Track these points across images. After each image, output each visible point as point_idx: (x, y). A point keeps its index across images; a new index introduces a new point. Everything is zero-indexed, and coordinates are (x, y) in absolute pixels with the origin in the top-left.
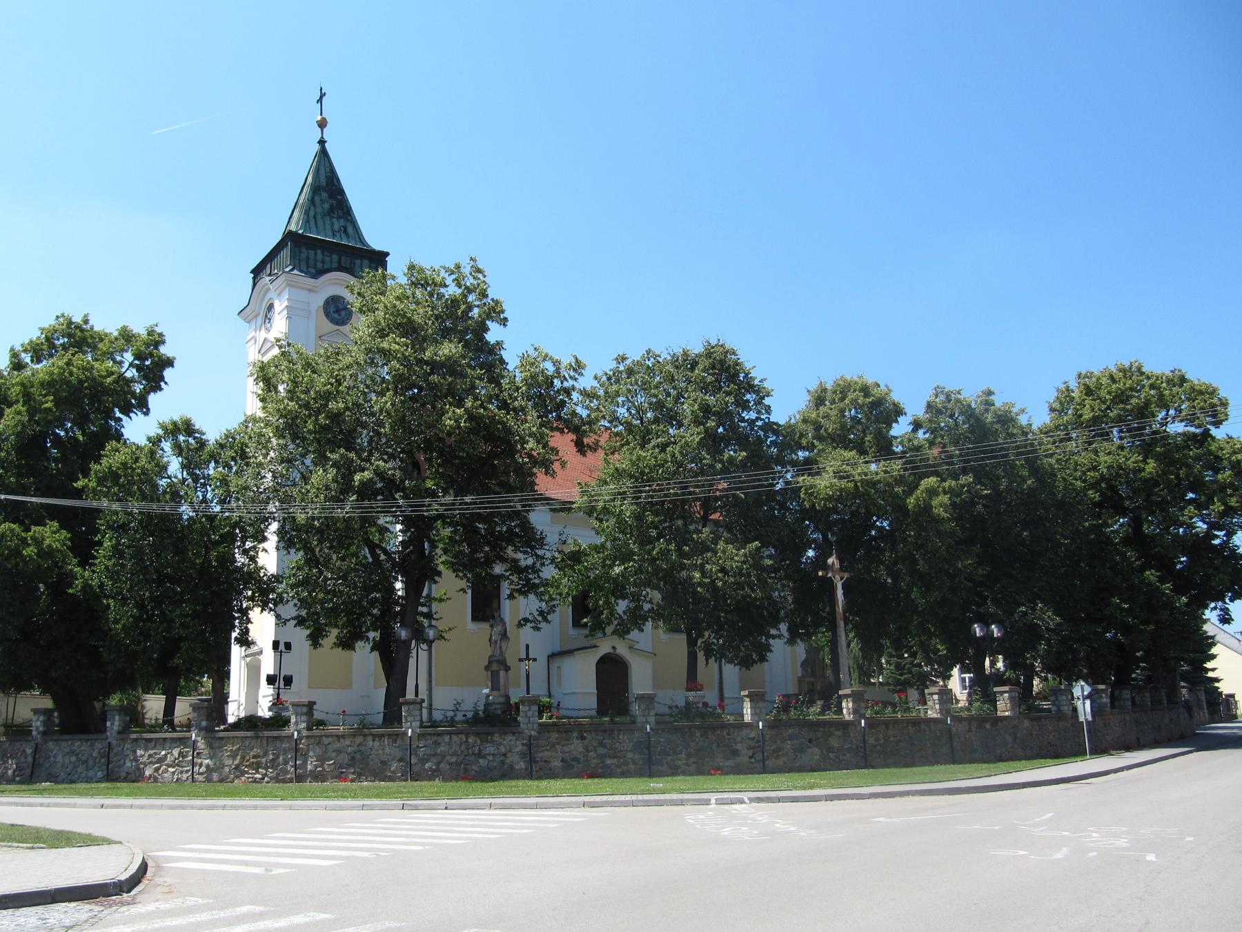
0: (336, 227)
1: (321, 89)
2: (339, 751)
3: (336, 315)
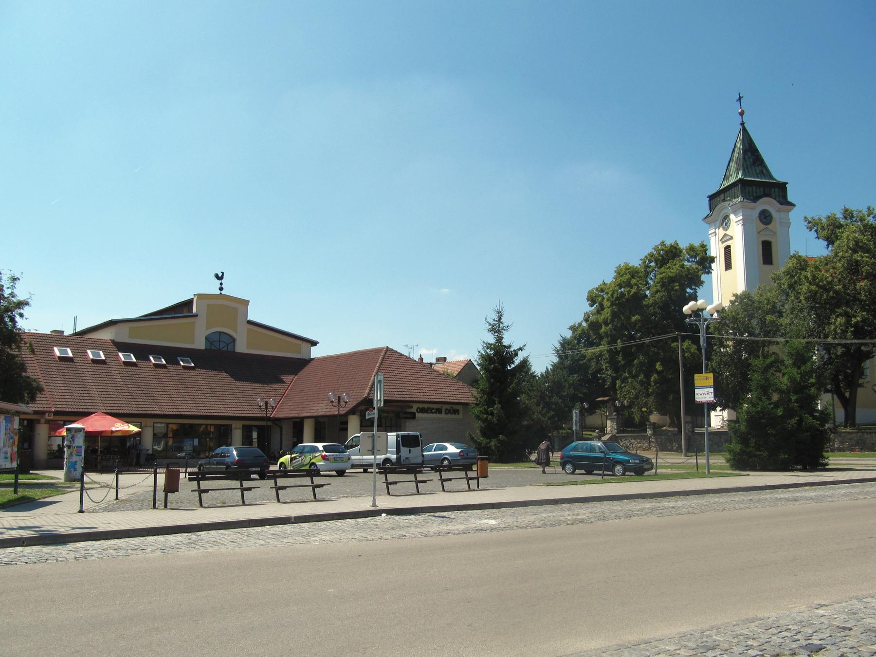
0: (758, 172)
1: (739, 94)
2: (851, 439)
3: (765, 220)
